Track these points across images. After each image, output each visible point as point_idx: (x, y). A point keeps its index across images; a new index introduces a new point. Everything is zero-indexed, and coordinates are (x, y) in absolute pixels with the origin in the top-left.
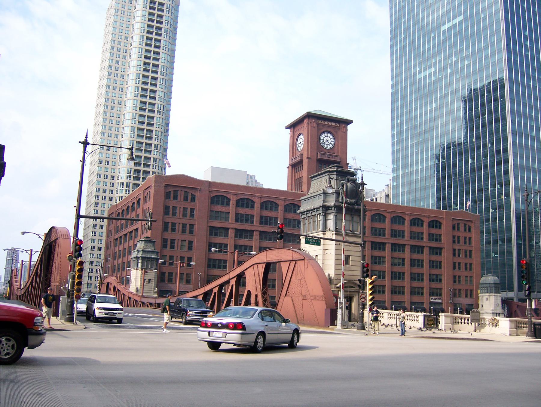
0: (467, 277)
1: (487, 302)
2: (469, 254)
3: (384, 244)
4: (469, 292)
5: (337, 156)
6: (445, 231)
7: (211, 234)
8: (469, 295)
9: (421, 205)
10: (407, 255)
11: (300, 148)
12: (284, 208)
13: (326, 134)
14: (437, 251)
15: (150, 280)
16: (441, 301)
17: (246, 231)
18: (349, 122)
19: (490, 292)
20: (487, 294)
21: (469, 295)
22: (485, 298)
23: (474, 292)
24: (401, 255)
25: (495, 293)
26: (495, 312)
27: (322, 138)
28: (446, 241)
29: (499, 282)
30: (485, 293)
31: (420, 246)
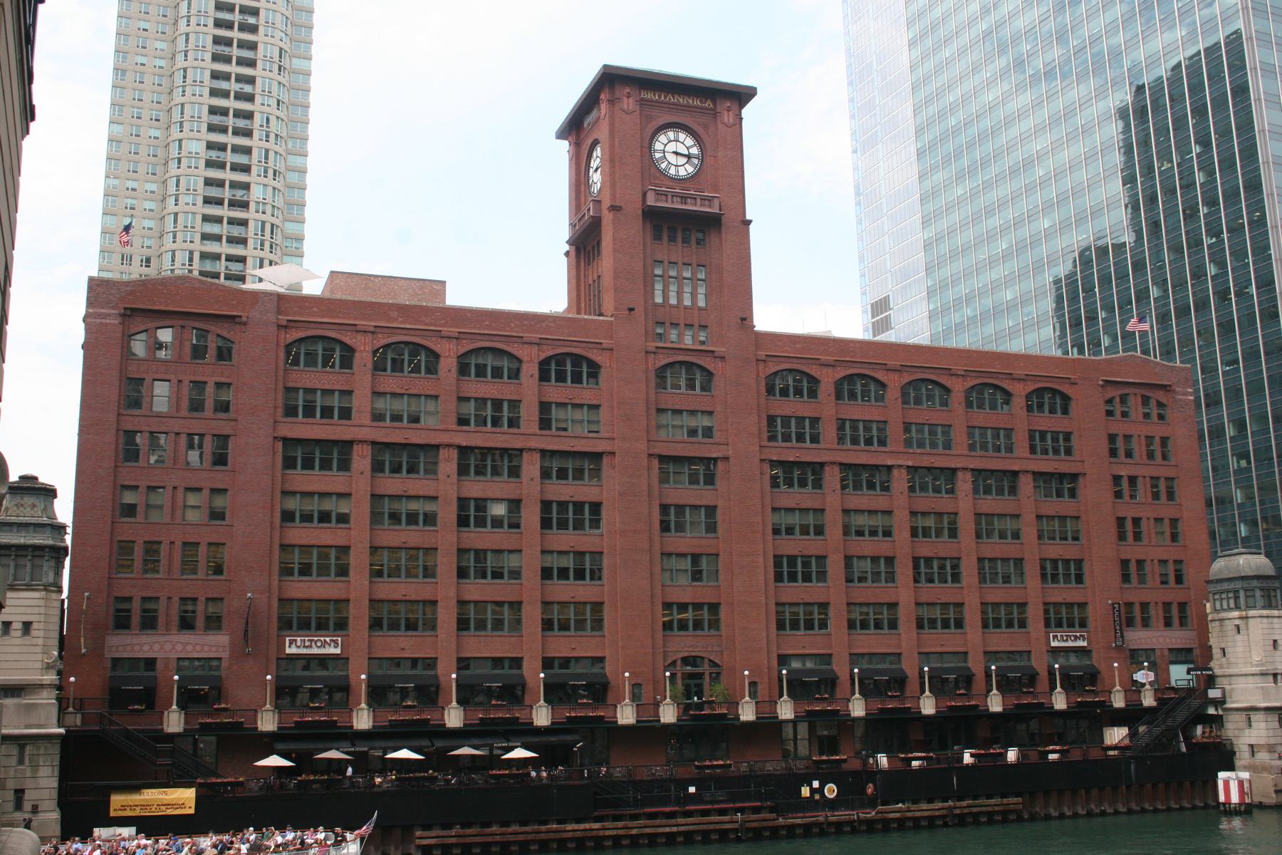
0: (1166, 561)
1: (1238, 637)
2: (1166, 489)
3: (818, 468)
4: (1175, 611)
5: (710, 200)
6: (1087, 421)
7: (289, 463)
8: (1176, 621)
9: (1016, 346)
10: (964, 501)
11: (596, 188)
12: (540, 370)
13: (671, 135)
14: (1065, 483)
15: (27, 626)
16: (1085, 644)
17: (325, 444)
18: (741, 95)
19: (1248, 607)
20: (1236, 614)
21: (1176, 621)
22: (1229, 626)
23: (1191, 611)
24: (943, 503)
25: (1264, 608)
26: (1270, 668)
27: (658, 146)
28: (1089, 456)
29: (1272, 572)
30: (1230, 609)
31: (504, 451)
